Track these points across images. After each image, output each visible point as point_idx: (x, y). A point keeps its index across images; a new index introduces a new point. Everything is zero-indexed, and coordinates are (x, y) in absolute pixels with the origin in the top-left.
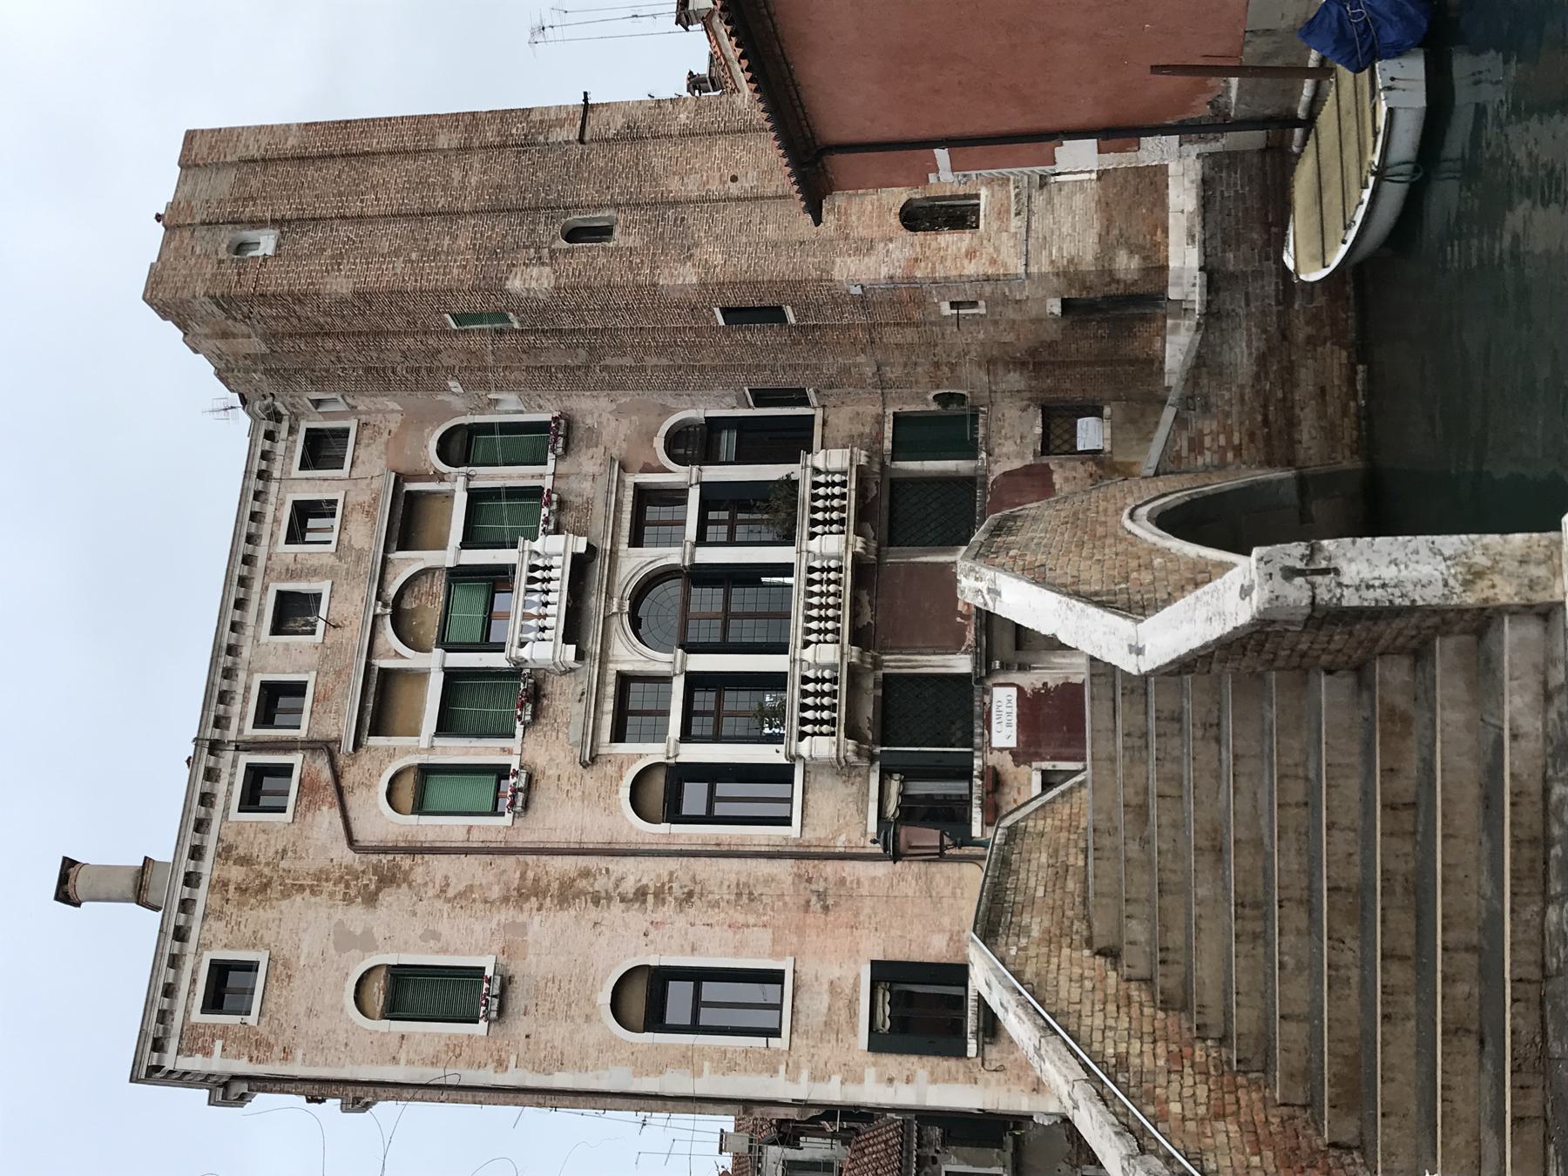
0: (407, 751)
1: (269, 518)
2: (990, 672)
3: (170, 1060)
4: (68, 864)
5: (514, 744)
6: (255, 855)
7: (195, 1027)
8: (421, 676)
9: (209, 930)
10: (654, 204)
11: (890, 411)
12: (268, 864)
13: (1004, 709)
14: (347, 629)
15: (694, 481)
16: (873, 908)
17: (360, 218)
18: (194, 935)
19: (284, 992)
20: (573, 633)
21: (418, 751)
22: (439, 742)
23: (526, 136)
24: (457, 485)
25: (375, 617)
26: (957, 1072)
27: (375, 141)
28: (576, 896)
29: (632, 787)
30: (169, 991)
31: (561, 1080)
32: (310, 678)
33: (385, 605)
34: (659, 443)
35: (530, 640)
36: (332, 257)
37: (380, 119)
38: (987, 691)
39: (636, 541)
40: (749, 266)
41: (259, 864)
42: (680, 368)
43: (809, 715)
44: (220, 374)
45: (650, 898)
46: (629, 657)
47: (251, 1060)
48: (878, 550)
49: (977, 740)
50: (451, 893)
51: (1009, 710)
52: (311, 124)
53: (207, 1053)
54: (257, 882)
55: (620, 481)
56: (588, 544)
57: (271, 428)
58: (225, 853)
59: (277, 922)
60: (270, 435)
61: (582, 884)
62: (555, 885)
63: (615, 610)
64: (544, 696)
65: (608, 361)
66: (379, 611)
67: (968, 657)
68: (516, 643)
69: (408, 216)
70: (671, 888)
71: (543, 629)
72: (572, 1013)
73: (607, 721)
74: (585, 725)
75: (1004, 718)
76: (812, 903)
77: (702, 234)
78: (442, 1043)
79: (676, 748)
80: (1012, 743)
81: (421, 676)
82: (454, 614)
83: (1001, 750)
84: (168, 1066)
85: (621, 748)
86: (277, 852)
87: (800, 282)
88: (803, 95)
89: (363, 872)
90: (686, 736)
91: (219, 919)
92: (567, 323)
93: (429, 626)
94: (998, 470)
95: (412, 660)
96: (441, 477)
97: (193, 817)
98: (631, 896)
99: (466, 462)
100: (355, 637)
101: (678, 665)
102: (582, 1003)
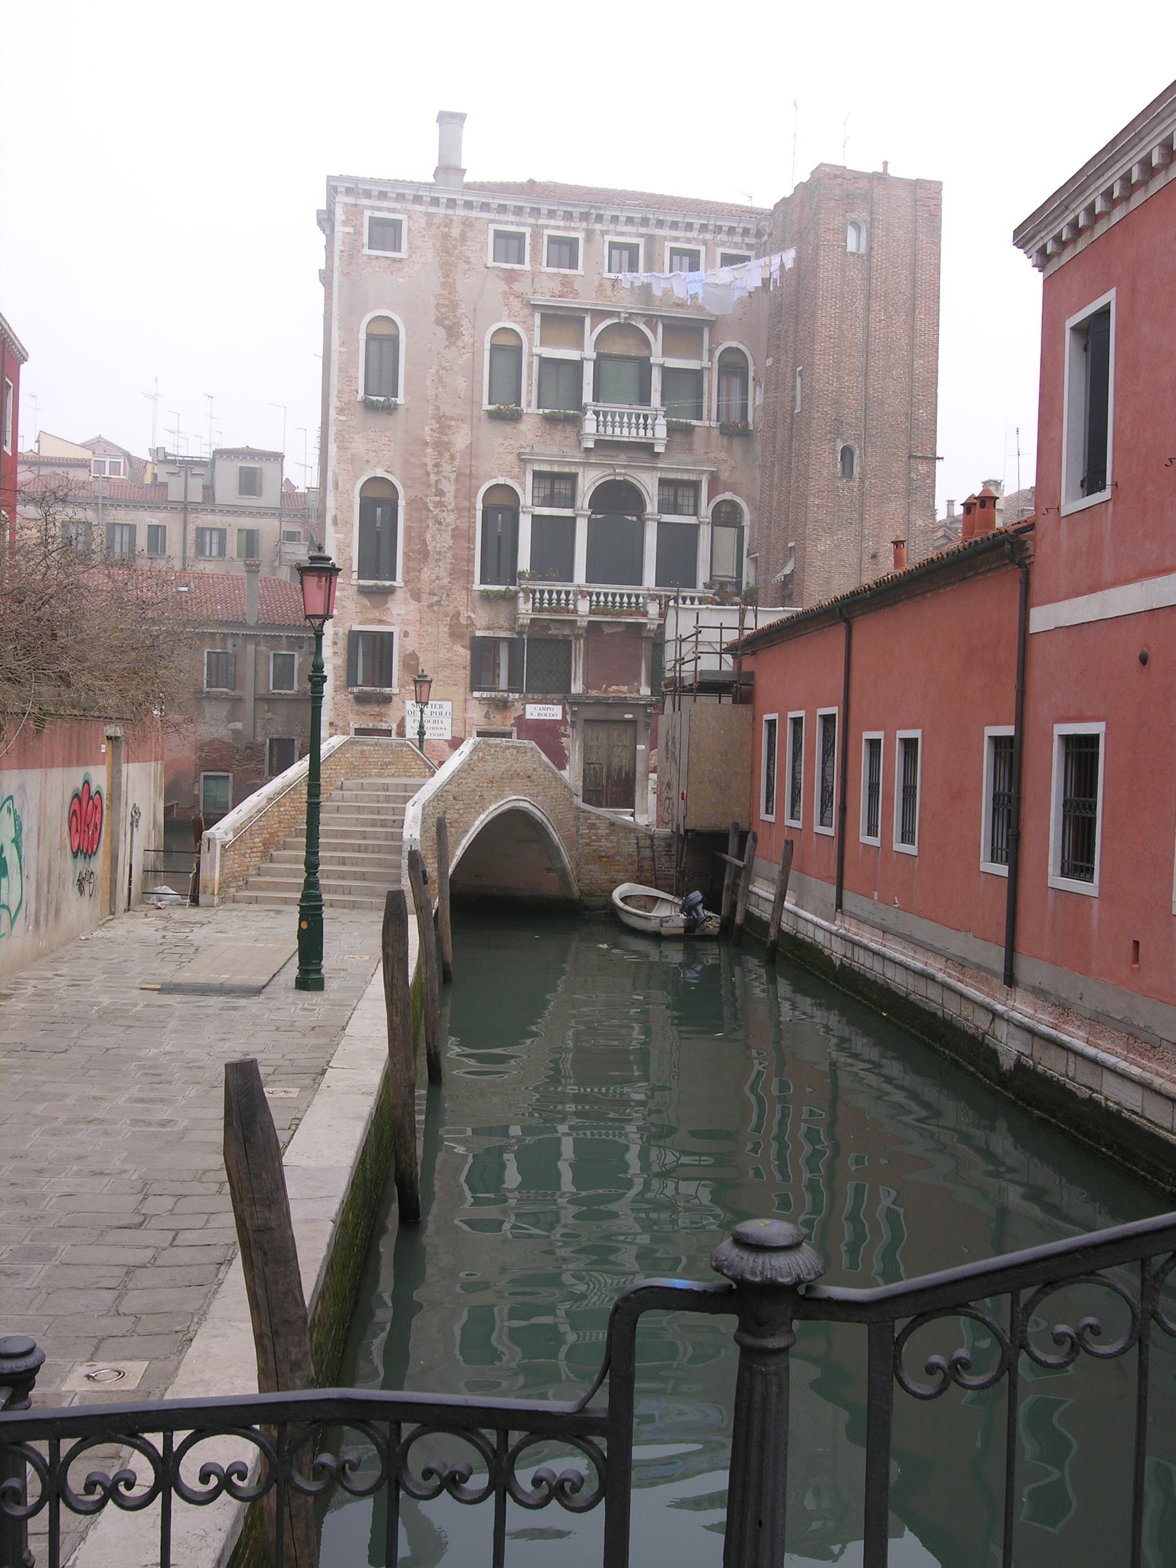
0: (531, 341)
1: (690, 235)
2: (572, 704)
3: (342, 199)
4: (462, 117)
5: (533, 409)
7: (362, 213)
8: (580, 346)
9: (420, 217)
10: (862, 505)
12: (460, 252)
18: (418, 208)
20: (602, 445)
21: (530, 348)
22: (536, 360)
23: (917, 419)
24: (704, 362)
25: (619, 313)
30: (383, 195)
31: (332, 448)
32: (580, 271)
33: (626, 318)
34: (728, 496)
37: (938, 319)
39: (663, 483)
40: (814, 567)
42: (771, 514)
43: (546, 596)
44: (784, 201)
45: (438, 499)
48: (650, 637)
49: (530, 696)
53: (345, 223)
57: (751, 232)
58: (467, 223)
60: (746, 232)
61: (447, 456)
62: (445, 439)
63: (617, 471)
65: (777, 467)
67: (581, 691)
69: (867, 343)
74: (543, 455)
75: (543, 712)
79: (528, 512)
80: (528, 716)
81: (580, 346)
83: (524, 710)
85: (529, 478)
86: (468, 258)
88: (872, 614)
90: (535, 518)
91: (427, 223)
92: (795, 445)
95: (590, 337)
96: (711, 352)
97: (491, 201)
98: (440, 486)
101: (580, 512)
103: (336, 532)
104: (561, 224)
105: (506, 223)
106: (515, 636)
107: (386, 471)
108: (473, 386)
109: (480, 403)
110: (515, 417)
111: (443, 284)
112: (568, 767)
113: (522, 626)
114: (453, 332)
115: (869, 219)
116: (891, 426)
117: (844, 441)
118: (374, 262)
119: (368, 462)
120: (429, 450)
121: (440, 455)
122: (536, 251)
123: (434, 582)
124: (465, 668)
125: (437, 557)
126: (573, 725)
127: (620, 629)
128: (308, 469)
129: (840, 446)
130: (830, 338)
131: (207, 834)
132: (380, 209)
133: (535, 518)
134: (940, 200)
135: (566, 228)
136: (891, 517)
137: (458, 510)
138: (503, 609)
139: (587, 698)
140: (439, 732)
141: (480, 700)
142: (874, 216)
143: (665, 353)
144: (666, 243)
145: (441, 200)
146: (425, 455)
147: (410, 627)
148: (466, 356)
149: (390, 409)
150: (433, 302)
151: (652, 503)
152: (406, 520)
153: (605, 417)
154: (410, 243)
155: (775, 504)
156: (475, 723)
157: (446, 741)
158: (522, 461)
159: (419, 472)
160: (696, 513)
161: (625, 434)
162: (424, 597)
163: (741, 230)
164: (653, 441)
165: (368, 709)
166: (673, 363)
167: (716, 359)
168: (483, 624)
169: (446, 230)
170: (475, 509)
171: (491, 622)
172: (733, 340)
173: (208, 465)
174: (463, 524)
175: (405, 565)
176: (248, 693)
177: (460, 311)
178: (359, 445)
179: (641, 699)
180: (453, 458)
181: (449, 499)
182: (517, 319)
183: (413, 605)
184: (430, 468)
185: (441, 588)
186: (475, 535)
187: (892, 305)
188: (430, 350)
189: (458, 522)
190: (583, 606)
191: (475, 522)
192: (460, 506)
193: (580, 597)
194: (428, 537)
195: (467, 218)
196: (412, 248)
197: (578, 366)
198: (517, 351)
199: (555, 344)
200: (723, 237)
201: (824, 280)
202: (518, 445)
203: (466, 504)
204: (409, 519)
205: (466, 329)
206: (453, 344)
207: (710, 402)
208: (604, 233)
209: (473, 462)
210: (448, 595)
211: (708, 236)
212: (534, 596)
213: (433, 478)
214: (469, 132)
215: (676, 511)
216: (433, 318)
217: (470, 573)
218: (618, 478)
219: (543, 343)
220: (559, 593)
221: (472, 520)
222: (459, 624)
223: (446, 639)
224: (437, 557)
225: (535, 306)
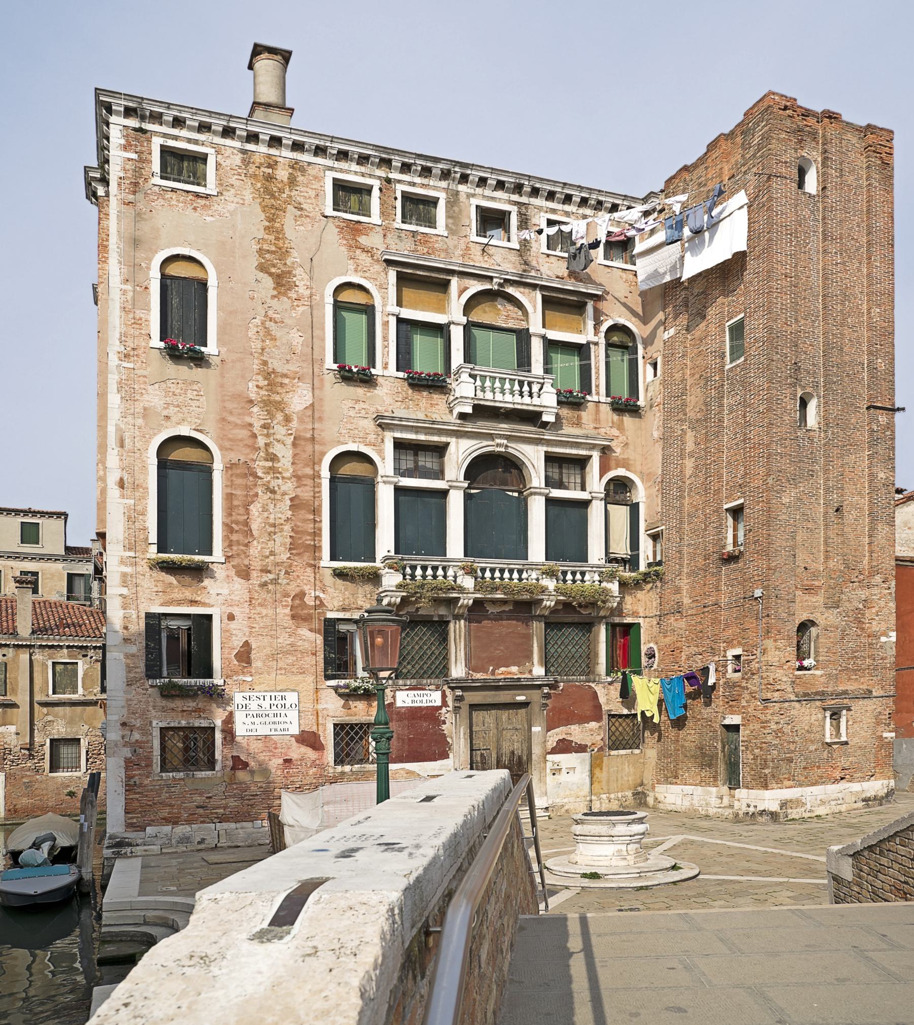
0: (384, 298)
1: (567, 208)
3: (118, 125)
6: (297, 188)
9: (233, 153)
11: (641, 621)
13: (424, 699)
14: (481, 258)
16: (266, 615)
18: (228, 142)
19: (181, 205)
20: (482, 412)
21: (384, 305)
22: (393, 321)
23: (876, 369)
25: (491, 278)
26: (136, 672)
27: (878, 265)
28: (269, 412)
29: (358, 452)
33: (500, 285)
34: (621, 472)
35: (476, 381)
38: (437, 689)
39: (550, 459)
41: (291, 191)
45: (270, 464)
46: (461, 450)
47: (121, 178)
48: (543, 616)
49: (401, 682)
50: (268, 324)
51: (424, 701)
52: (893, 220)
53: (125, 148)
54: (275, 189)
55: (593, 447)
58: (295, 165)
59: (241, 202)
61: (279, 417)
67: (464, 675)
70: (278, 478)
72: (172, 408)
74: (408, 420)
75: (418, 699)
76: (269, 575)
77: (802, 489)
78: (142, 316)
79: (390, 483)
80: (399, 704)
82: (491, 334)
83: (394, 697)
84: (113, 119)
85: (389, 447)
86: (300, 204)
89: (285, 264)
93: (481, 315)
94: (600, 690)
97: (328, 144)
98: (271, 450)
99: (609, 345)
100: (478, 261)
102: (180, 415)
104: (418, 180)
109: (322, 361)
110: (365, 379)
111: (267, 228)
112: (451, 755)
117: (803, 388)
118: (169, 195)
119: (167, 418)
121: (272, 416)
123: (268, 557)
124: (315, 654)
129: (800, 393)
132: (176, 138)
135: (423, 186)
137: (298, 478)
140: (282, 726)
141: (336, 689)
144: (542, 214)
146: (250, 414)
147: (236, 608)
149: (199, 360)
153: (483, 382)
156: (331, 714)
157: (292, 736)
159: (244, 433)
161: (508, 400)
162: (254, 574)
164: (541, 409)
165: (178, 704)
167: (602, 335)
168: (336, 604)
169: (270, 171)
170: (319, 477)
171: (347, 602)
175: (226, 538)
178: (154, 398)
179: (533, 679)
180: (287, 419)
181: (285, 462)
182: (367, 275)
183: (239, 584)
184: (257, 429)
192: (300, 473)
195: (297, 162)
196: (220, 182)
204: (229, 484)
205: (301, 278)
207: (597, 378)
208: (469, 196)
209: (316, 426)
210: (287, 573)
215: (561, 485)
217: (317, 548)
221: (317, 490)
222: (304, 605)
225: (389, 263)
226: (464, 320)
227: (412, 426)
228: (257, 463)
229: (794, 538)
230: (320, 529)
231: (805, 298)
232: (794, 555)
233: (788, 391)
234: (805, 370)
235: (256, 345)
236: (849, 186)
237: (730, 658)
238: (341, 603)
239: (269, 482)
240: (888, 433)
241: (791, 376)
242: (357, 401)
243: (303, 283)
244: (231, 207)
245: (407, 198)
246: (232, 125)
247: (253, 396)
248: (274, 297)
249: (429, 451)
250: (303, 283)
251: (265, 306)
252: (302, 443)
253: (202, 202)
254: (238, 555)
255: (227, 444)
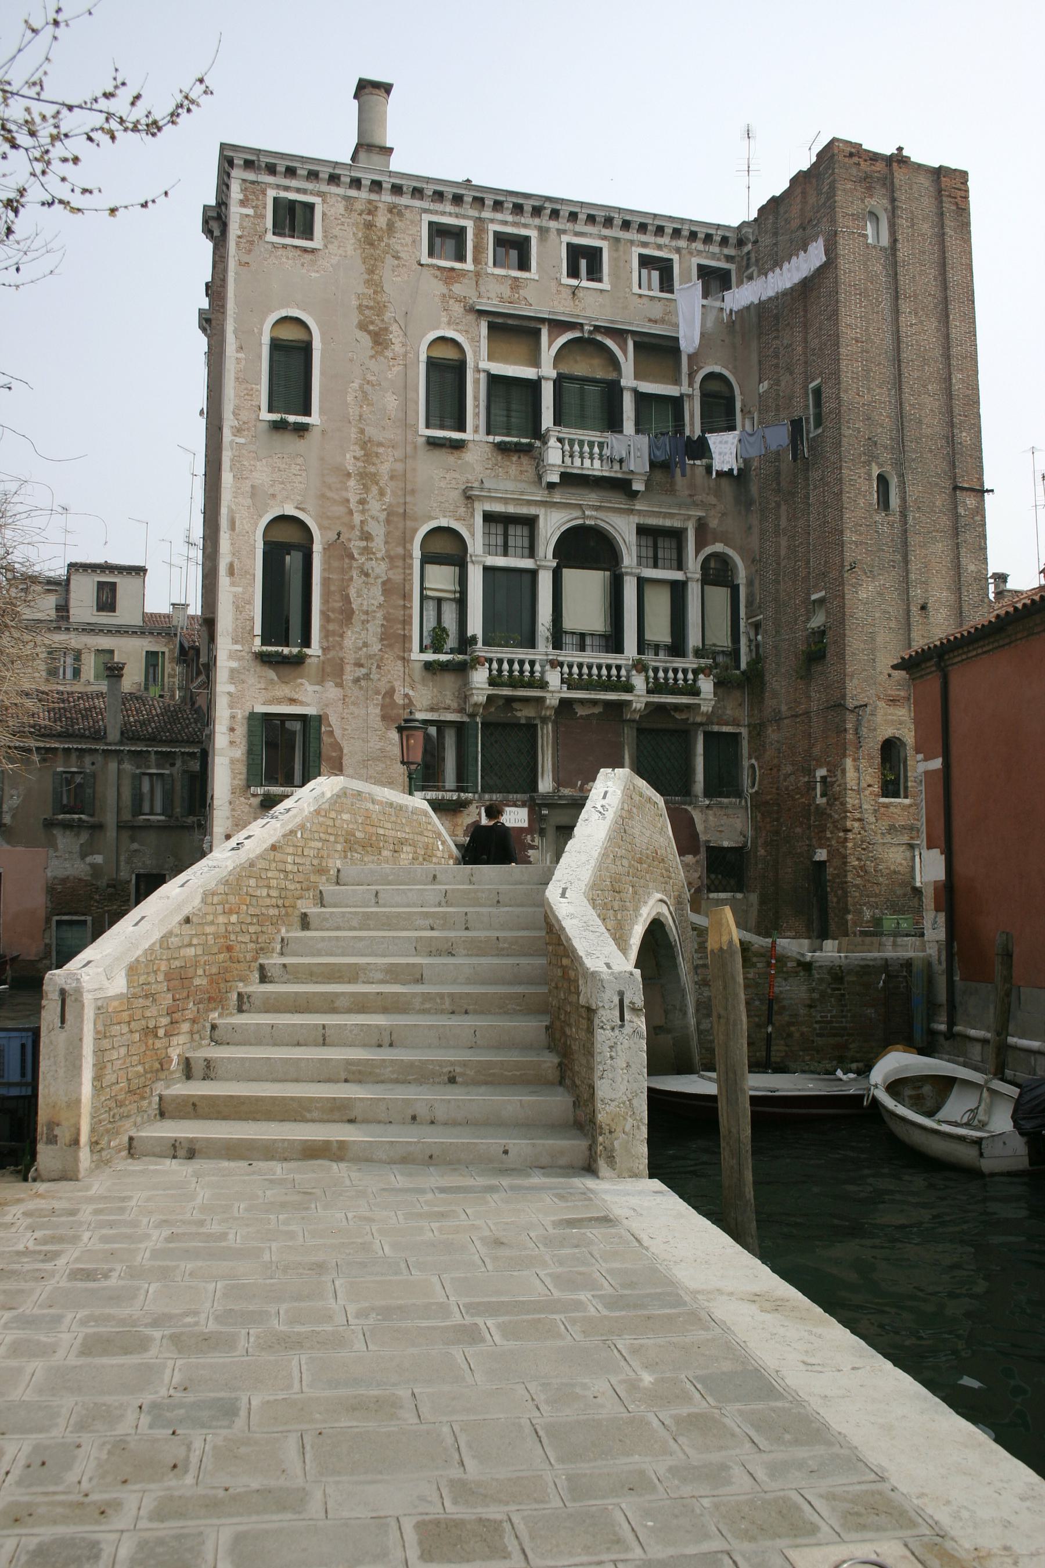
0: (477, 353)
1: (660, 240)
8: (536, 362)
12: (388, 245)
15: (689, 575)
17: (896, 312)
18: (334, 189)
19: (290, 262)
20: (570, 480)
22: (483, 377)
23: (960, 443)
25: (582, 325)
30: (291, 172)
32: (534, 273)
33: (590, 332)
34: (718, 547)
36: (866, 289)
39: (642, 531)
42: (778, 564)
44: (774, 203)
45: (363, 543)
48: (634, 721)
53: (243, 203)
56: (639, 491)
61: (375, 490)
64: (519, 458)
66: (586, 328)
67: (551, 790)
68: (561, 435)
70: (371, 559)
71: (571, 456)
73: (498, 508)
79: (479, 562)
85: (479, 520)
86: (398, 252)
87: (844, 658)
89: (383, 320)
96: (691, 376)
97: (425, 186)
98: (366, 528)
101: (543, 563)
103: (233, 584)
105: (443, 213)
106: (466, 719)
107: (297, 508)
108: (406, 403)
109: (416, 426)
113: (476, 705)
114: (379, 340)
115: (889, 207)
116: (931, 451)
117: (880, 466)
118: (280, 252)
119: (273, 496)
120: (352, 483)
122: (478, 249)
123: (361, 649)
125: (364, 617)
126: (542, 833)
127: (597, 710)
128: (176, 571)
129: (876, 472)
130: (857, 341)
131: (56, 978)
132: (287, 188)
133: (487, 569)
134: (967, 191)
135: (515, 224)
136: (938, 560)
137: (390, 558)
138: (450, 681)
139: (560, 797)
142: (896, 203)
143: (637, 377)
144: (634, 248)
145: (363, 182)
146: (346, 489)
148: (396, 369)
150: (355, 303)
151: (630, 555)
152: (324, 570)
153: (571, 446)
154: (325, 231)
155: (783, 553)
158: (469, 498)
159: (340, 510)
160: (680, 567)
161: (595, 468)
162: (348, 668)
163: (719, 239)
164: (630, 477)
166: (648, 387)
167: (697, 385)
169: (370, 218)
170: (411, 557)
172: (716, 364)
173: (61, 586)
174: (397, 576)
175: (323, 628)
176: (110, 819)
177: (388, 315)
180: (382, 493)
181: (378, 544)
182: (460, 327)
185: (370, 657)
186: (411, 590)
187: (922, 309)
188: (351, 360)
189: (391, 574)
190: (553, 678)
191: (411, 574)
192: (392, 553)
193: (548, 667)
194: (352, 592)
197: (533, 387)
198: (459, 368)
199: (505, 360)
200: (698, 245)
201: (845, 273)
202: (465, 480)
203: (400, 550)
204: (327, 568)
205: (395, 335)
206: (381, 353)
209: (408, 499)
210: (379, 667)
211: (682, 243)
212: (490, 665)
213: (357, 518)
214: (394, 106)
216: (356, 322)
217: (406, 639)
218: (588, 522)
219: (491, 358)
220: (521, 663)
221: (407, 571)
222: (393, 704)
223: (376, 721)
224: (364, 617)
225: (481, 313)
226: (554, 374)
227: (501, 498)
228: (353, 543)
229: (873, 639)
230: (411, 617)
231: (879, 364)
232: (874, 660)
233: (863, 470)
234: (883, 446)
235: (353, 412)
236: (922, 235)
237: (818, 779)
238: (429, 702)
239: (363, 564)
240: (978, 518)
241: (864, 454)
242: (448, 470)
243: (399, 340)
244: (335, 260)
245: (501, 240)
246: (337, 171)
247: (351, 469)
248: (372, 357)
249: (519, 523)
250: (399, 340)
251: (363, 368)
252: (395, 519)
253: (308, 257)
254: (334, 647)
255: (326, 523)
